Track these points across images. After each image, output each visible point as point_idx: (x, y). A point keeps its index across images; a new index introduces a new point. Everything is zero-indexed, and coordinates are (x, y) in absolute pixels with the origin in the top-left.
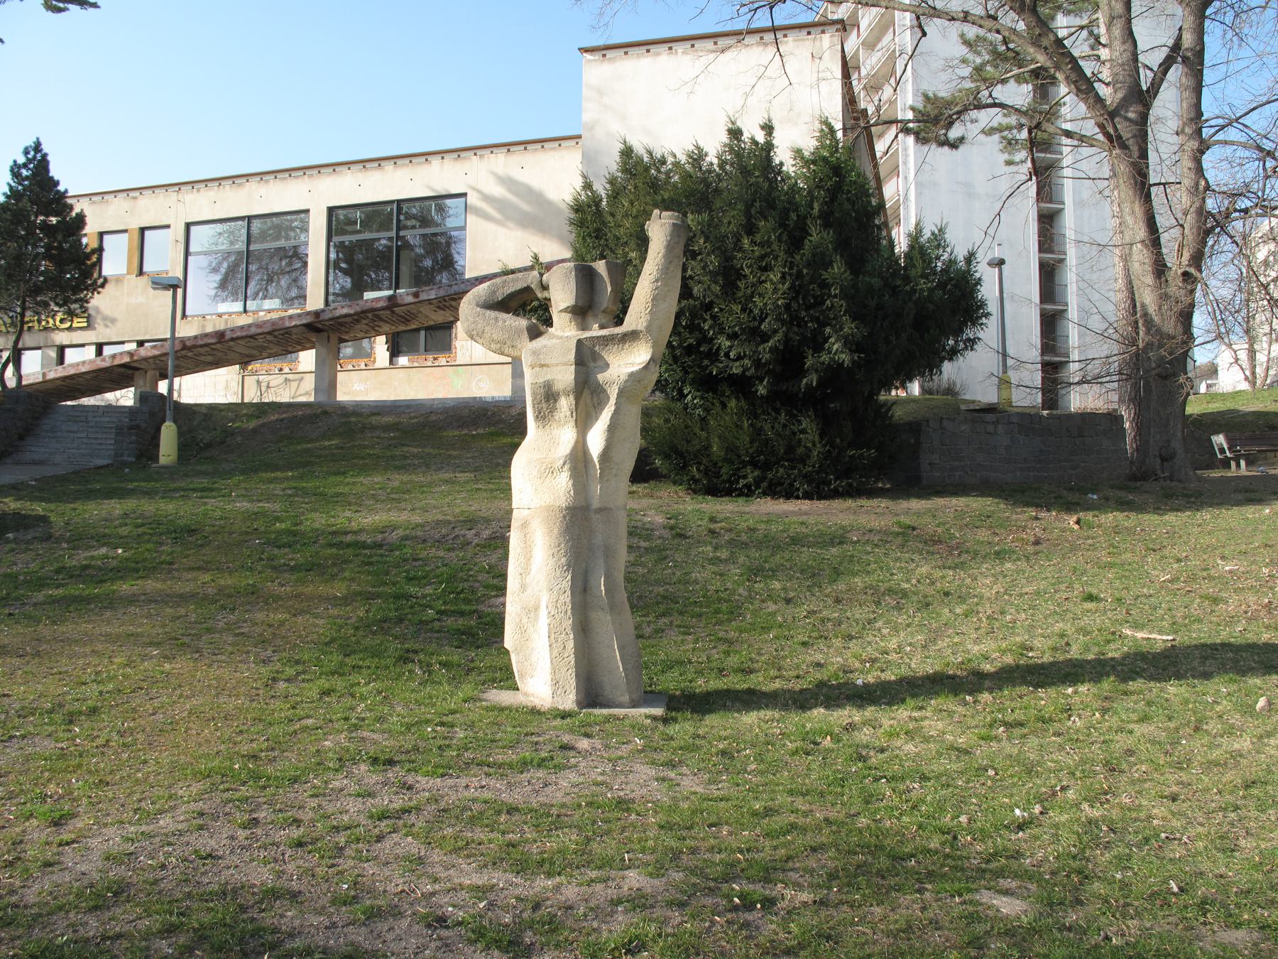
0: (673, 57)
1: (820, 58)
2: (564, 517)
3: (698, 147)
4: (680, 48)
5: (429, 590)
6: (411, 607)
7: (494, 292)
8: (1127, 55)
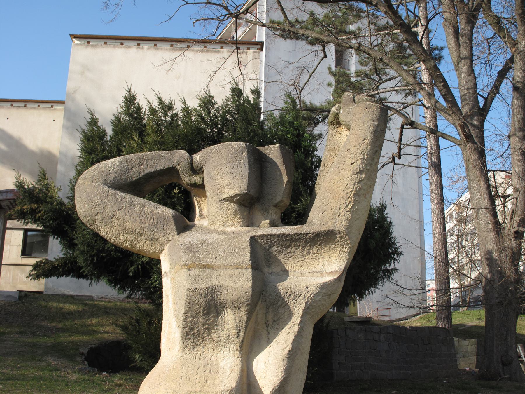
0: (140, 51)
1: (245, 66)
4: (145, 46)
7: (127, 170)
8: (471, 84)
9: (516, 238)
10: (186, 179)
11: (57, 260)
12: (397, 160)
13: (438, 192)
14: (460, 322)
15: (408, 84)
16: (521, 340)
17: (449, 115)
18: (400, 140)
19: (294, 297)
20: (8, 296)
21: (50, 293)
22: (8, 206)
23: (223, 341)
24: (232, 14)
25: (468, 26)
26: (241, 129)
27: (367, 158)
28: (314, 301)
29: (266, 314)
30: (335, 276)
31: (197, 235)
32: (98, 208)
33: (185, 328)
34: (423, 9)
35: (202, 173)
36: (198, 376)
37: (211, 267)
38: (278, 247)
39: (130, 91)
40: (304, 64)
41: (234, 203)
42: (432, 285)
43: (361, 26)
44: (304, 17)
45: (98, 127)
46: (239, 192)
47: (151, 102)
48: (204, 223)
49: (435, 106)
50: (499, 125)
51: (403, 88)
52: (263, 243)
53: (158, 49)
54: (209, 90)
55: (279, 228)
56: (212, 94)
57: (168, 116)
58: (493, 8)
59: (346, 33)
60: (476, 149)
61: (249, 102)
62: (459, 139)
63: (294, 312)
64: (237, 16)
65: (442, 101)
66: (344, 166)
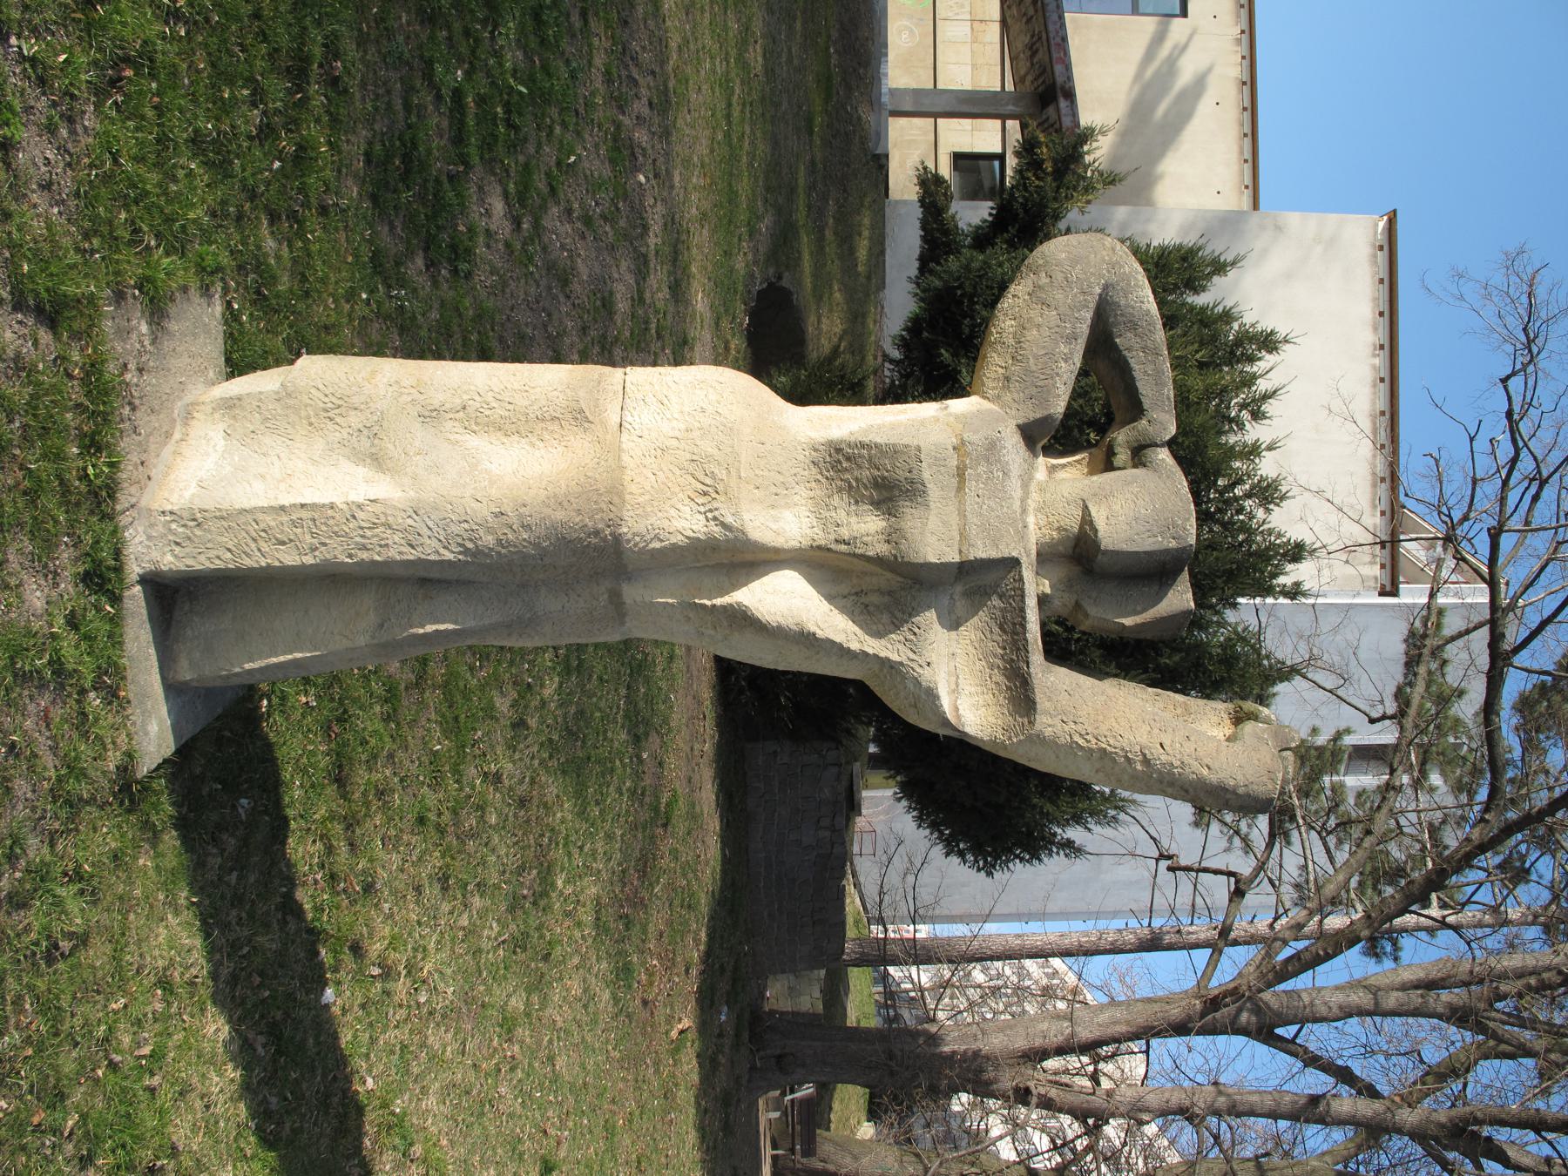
1: (1347, 562)
2: (597, 533)
3: (1283, 498)
4: (1380, 361)
5: (513, 58)
6: (467, 33)
7: (1133, 326)
8: (1323, 1011)
9: (1017, 1090)
10: (1122, 437)
11: (953, 217)
12: (1164, 864)
13: (1103, 944)
14: (852, 987)
15: (1318, 889)
16: (822, 1098)
17: (1258, 967)
18: (1206, 870)
19: (911, 641)
20: (878, 134)
21: (887, 210)
22: (1048, 119)
23: (828, 514)
24: (1454, 530)
25: (1445, 1007)
26: (1217, 559)
27: (1174, 774)
28: (904, 677)
29: (880, 592)
30: (950, 716)
31: (1019, 460)
32: (1060, 276)
33: (849, 445)
34: (1480, 921)
35: (1135, 466)
36: (766, 473)
37: (960, 488)
38: (1001, 610)
39: (1286, 341)
40: (1356, 677)
41: (1081, 527)
42: (923, 931)
43: (1439, 792)
44: (1453, 677)
45: (1209, 277)
46: (1100, 534)
47: (1267, 376)
48: (1041, 474)
49: (1275, 939)
50: (1241, 1066)
51: (1312, 878)
52: (1008, 583)
53: (1374, 386)
54: (1294, 497)
55: (1036, 610)
56: (1284, 504)
57: (1240, 411)
58: (1486, 1063)
59: (1423, 763)
60: (1190, 1018)
61: (1274, 576)
62: (1210, 986)
63: (883, 642)
64: (1448, 539)
65: (1287, 953)
66: (1156, 731)
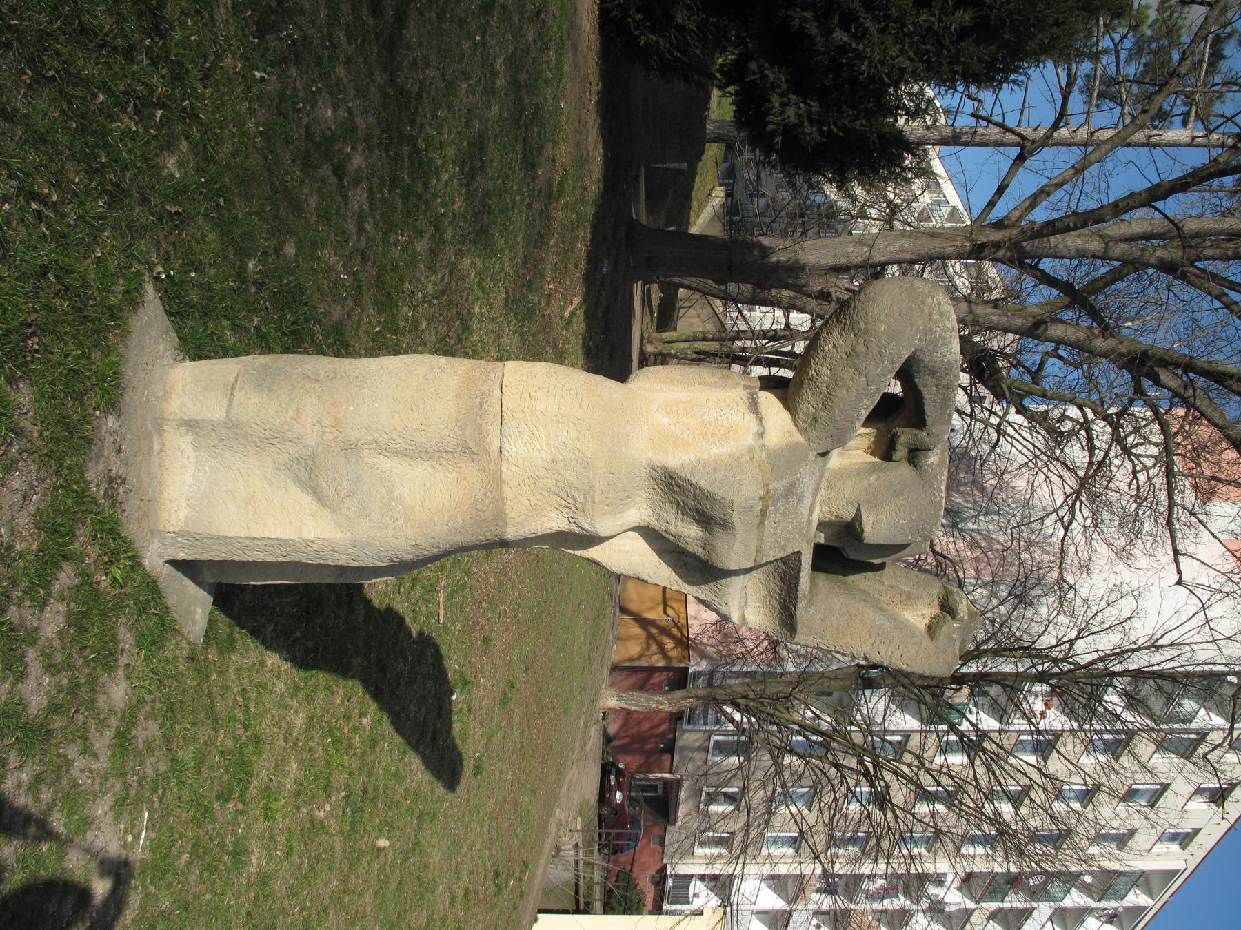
8: (1065, 252)
37: (761, 523)
